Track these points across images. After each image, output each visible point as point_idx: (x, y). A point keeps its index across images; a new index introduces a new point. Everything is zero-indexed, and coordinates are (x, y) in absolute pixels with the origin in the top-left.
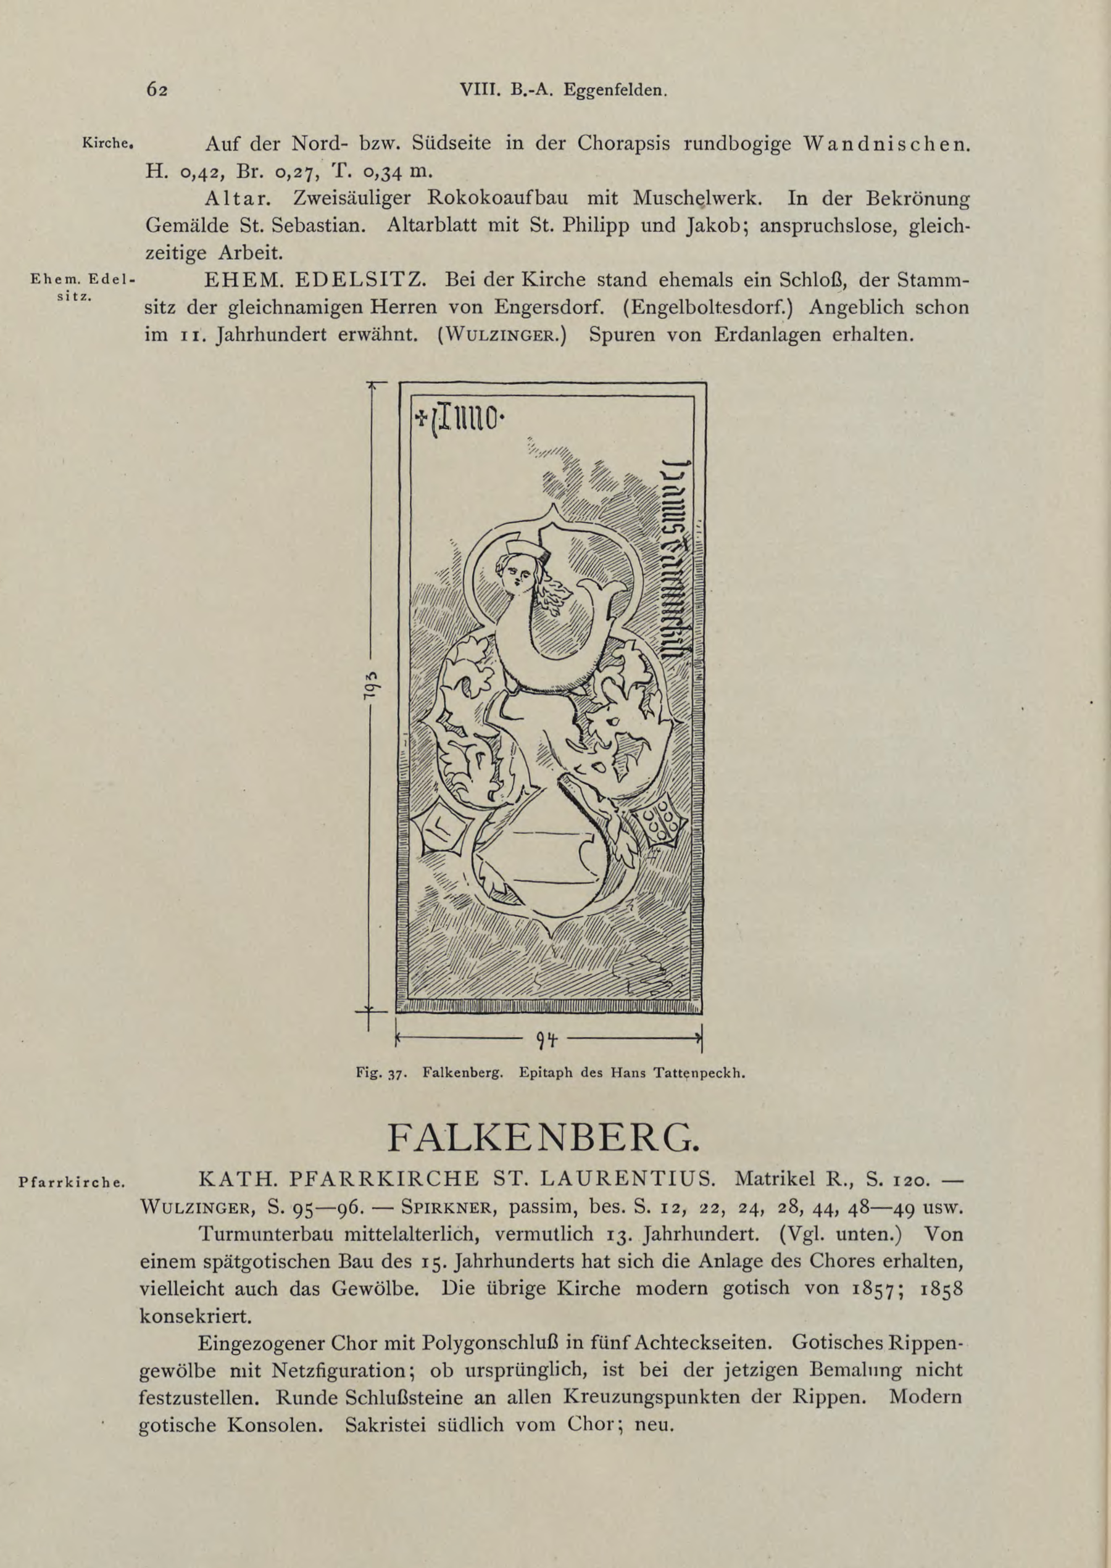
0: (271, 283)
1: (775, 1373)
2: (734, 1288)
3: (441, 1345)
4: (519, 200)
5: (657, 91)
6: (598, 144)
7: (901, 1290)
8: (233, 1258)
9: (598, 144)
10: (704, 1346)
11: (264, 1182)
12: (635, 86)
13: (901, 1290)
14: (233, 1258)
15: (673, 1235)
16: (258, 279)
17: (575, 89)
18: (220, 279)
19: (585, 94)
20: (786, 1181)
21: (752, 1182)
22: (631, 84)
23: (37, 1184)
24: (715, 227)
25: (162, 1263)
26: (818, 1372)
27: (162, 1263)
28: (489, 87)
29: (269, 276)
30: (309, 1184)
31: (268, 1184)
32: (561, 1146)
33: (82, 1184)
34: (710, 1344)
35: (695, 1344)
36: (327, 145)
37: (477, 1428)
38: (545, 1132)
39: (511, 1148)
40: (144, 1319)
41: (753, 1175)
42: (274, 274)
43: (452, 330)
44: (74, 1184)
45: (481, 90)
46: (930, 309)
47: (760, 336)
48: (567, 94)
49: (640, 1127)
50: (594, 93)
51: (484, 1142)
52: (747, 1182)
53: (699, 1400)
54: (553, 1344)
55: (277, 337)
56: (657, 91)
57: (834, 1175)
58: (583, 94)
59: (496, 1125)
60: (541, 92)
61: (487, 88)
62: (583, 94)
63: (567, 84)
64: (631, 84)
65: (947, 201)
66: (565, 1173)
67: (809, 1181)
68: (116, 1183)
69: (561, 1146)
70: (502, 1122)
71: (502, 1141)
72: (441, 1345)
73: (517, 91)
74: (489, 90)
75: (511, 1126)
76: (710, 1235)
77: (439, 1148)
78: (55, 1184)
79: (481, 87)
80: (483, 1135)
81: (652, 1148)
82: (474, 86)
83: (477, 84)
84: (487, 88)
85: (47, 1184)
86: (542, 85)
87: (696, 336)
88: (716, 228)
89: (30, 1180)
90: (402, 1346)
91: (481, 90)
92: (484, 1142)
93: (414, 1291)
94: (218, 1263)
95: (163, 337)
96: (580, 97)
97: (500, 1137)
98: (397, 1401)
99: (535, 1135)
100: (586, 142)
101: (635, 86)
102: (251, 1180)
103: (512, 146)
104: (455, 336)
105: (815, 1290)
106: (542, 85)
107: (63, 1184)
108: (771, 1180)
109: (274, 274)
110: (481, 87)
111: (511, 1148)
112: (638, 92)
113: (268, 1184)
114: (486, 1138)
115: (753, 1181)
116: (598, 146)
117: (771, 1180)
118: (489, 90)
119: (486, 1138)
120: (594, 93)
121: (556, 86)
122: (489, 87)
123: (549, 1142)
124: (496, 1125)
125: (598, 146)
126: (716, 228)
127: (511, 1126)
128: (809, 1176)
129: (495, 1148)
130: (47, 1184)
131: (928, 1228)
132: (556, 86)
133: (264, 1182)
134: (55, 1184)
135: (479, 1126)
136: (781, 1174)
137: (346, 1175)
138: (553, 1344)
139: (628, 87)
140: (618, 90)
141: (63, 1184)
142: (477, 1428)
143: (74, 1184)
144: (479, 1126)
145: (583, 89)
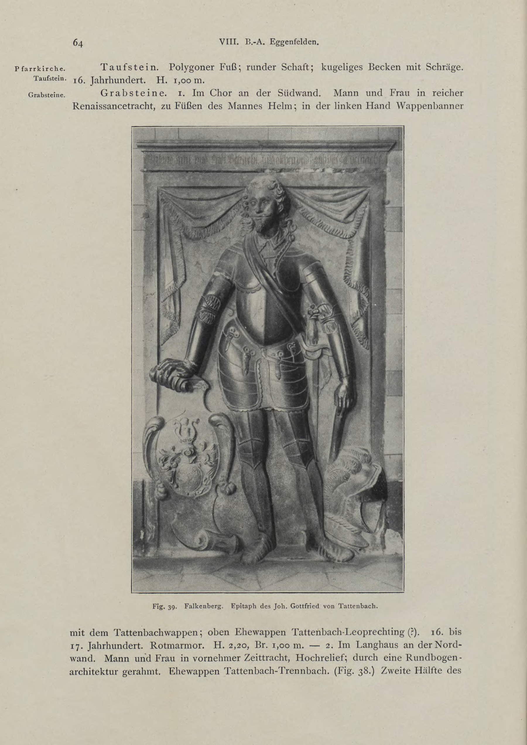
1: (455, 69)
2: (194, 67)
3: (178, 68)
4: (391, 646)
5: (314, 42)
6: (220, 93)
7: (312, 68)
9: (220, 93)
13: (312, 68)
15: (442, 67)
17: (275, 41)
19: (280, 44)
23: (24, 70)
26: (372, 68)
28: (233, 40)
33: (45, 69)
35: (383, 68)
36: (452, 645)
40: (323, 69)
44: (42, 69)
45: (229, 42)
54: (234, 68)
56: (314, 42)
58: (281, 44)
60: (259, 43)
61: (233, 41)
62: (281, 44)
65: (256, 68)
72: (178, 68)
73: (248, 43)
74: (233, 42)
78: (32, 70)
82: (226, 41)
84: (233, 41)
90: (415, 68)
91: (229, 42)
93: (461, 68)
98: (231, 69)
100: (214, 93)
103: (183, 660)
107: (36, 70)
110: (229, 40)
112: (305, 42)
116: (220, 94)
118: (233, 42)
122: (233, 40)
125: (220, 94)
130: (29, 70)
134: (32, 70)
138: (234, 68)
139: (300, 40)
141: (36, 70)
143: (42, 69)
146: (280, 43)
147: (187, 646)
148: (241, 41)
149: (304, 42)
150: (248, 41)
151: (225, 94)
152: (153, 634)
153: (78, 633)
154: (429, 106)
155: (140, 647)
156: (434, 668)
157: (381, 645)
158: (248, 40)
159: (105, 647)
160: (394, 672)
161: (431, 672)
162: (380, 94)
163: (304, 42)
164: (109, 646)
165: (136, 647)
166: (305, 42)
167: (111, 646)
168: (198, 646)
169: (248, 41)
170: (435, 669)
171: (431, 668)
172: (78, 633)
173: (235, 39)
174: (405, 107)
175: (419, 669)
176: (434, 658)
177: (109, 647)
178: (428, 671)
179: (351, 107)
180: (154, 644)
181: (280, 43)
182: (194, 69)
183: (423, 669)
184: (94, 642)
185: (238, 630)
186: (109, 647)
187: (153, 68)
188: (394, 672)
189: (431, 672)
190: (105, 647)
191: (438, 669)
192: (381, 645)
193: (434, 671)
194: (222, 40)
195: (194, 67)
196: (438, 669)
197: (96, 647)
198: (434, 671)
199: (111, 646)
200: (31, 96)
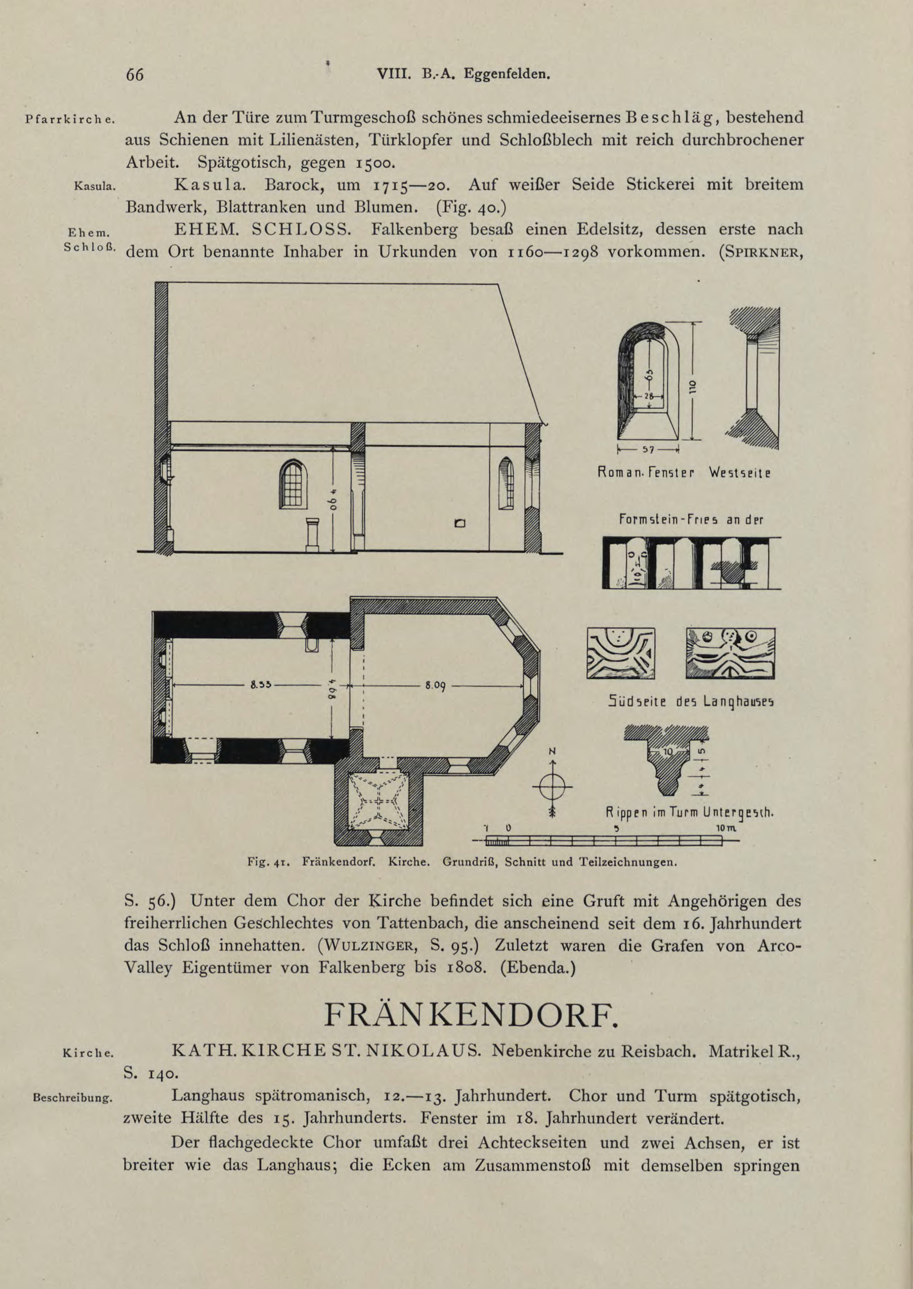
0: (229, 232)
2: (240, 163)
5: (542, 75)
6: (304, 901)
8: (279, 1093)
9: (304, 901)
10: (536, 1145)
11: (225, 1053)
12: (524, 70)
14: (279, 1093)
16: (218, 228)
17: (473, 73)
18: (187, 228)
19: (482, 77)
20: (750, 1054)
21: (723, 1054)
22: (520, 69)
23: (40, 120)
24: (287, 208)
25: (560, 902)
27: (560, 902)
28: (401, 72)
29: (227, 226)
30: (330, 1024)
31: (229, 1055)
32: (500, 1022)
33: (78, 120)
34: (540, 1143)
37: (291, 142)
38: (487, 1010)
39: (461, 1023)
41: (724, 1049)
42: (231, 224)
43: (330, 942)
44: (72, 120)
46: (273, 164)
47: (191, 1097)
48: (467, 77)
49: (573, 1007)
50: (490, 77)
51: (438, 1019)
52: (719, 1054)
53: (279, 209)
55: (626, 1098)
56: (542, 75)
57: (784, 1048)
58: (484, 77)
59: (447, 1004)
62: (484, 77)
63: (466, 69)
64: (520, 69)
66: (195, 1046)
67: (769, 1053)
68: (453, 78)
69: (500, 1022)
70: (453, 1001)
71: (453, 1017)
73: (428, 75)
74: (401, 74)
75: (461, 1004)
76: (631, 1097)
77: (393, 1024)
78: (55, 121)
79: (394, 72)
80: (437, 1012)
81: (583, 1025)
82: (388, 72)
83: (391, 69)
84: (401, 73)
85: (49, 120)
86: (446, 70)
87: (366, 924)
88: (412, 1168)
89: (34, 117)
91: (395, 74)
92: (438, 1019)
94: (267, 1097)
95: (273, 903)
96: (478, 80)
97: (452, 1014)
99: (479, 1012)
101: (524, 70)
102: (216, 1051)
104: (332, 947)
105: (724, 948)
106: (446, 70)
107: (62, 121)
108: (738, 1053)
109: (231, 224)
110: (394, 72)
111: (461, 1023)
112: (526, 75)
113: (229, 1055)
114: (439, 1015)
115: (724, 1053)
116: (586, 1098)
117: (738, 1053)
118: (401, 74)
119: (439, 1015)
120: (490, 77)
121: (457, 70)
122: (401, 72)
123: (491, 1019)
124: (447, 1004)
125: (586, 1098)
126: (412, 1168)
127: (461, 1004)
128: (769, 1049)
129: (447, 1023)
130: (49, 120)
131: (446, 1055)
132: (457, 70)
133: (225, 1053)
134: (55, 121)
135: (434, 1004)
136: (746, 1048)
137: (273, 1047)
139: (518, 71)
140: (509, 74)
141: (62, 121)
142: (291, 142)
143: (72, 120)
144: (434, 1004)
145: (480, 73)
146: (482, 75)
147: (688, 1097)
148: (415, 72)
149: (528, 74)
150: (427, 73)
151: (596, 1097)
152: (445, 925)
153: (616, 141)
154: (720, 140)
155: (546, 1097)
156: (214, 1114)
157: (215, 1096)
158: (427, 71)
159: (576, 1119)
160: (142, 1120)
161: (209, 1120)
162: (340, 209)
163: (528, 74)
164: (491, 1096)
165: (713, 1120)
166: (526, 75)
167: (586, 1119)
168: (601, 1096)
169: (427, 73)
170: (217, 1116)
171: (209, 1114)
172: (616, 141)
173: (404, 69)
174: (340, 946)
175: (188, 1114)
176: (700, 1167)
177: (582, 1120)
178: (204, 1119)
179: (287, 208)
180: (628, 1048)
181: (482, 75)
182: (240, 165)
183: (195, 1115)
184: (721, 917)
185: (187, 965)
186: (582, 1120)
187: (101, 234)
188: (142, 1120)
189: (209, 1120)
190: (486, 1097)
191: (221, 1115)
192: (215, 1096)
193: (214, 1119)
194: (383, 71)
195: (240, 163)
196: (221, 1115)
197: (318, 1119)
198: (214, 1119)
199: (586, 1119)
200: (589, 903)
